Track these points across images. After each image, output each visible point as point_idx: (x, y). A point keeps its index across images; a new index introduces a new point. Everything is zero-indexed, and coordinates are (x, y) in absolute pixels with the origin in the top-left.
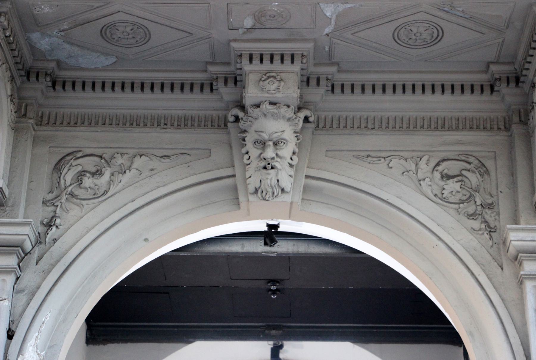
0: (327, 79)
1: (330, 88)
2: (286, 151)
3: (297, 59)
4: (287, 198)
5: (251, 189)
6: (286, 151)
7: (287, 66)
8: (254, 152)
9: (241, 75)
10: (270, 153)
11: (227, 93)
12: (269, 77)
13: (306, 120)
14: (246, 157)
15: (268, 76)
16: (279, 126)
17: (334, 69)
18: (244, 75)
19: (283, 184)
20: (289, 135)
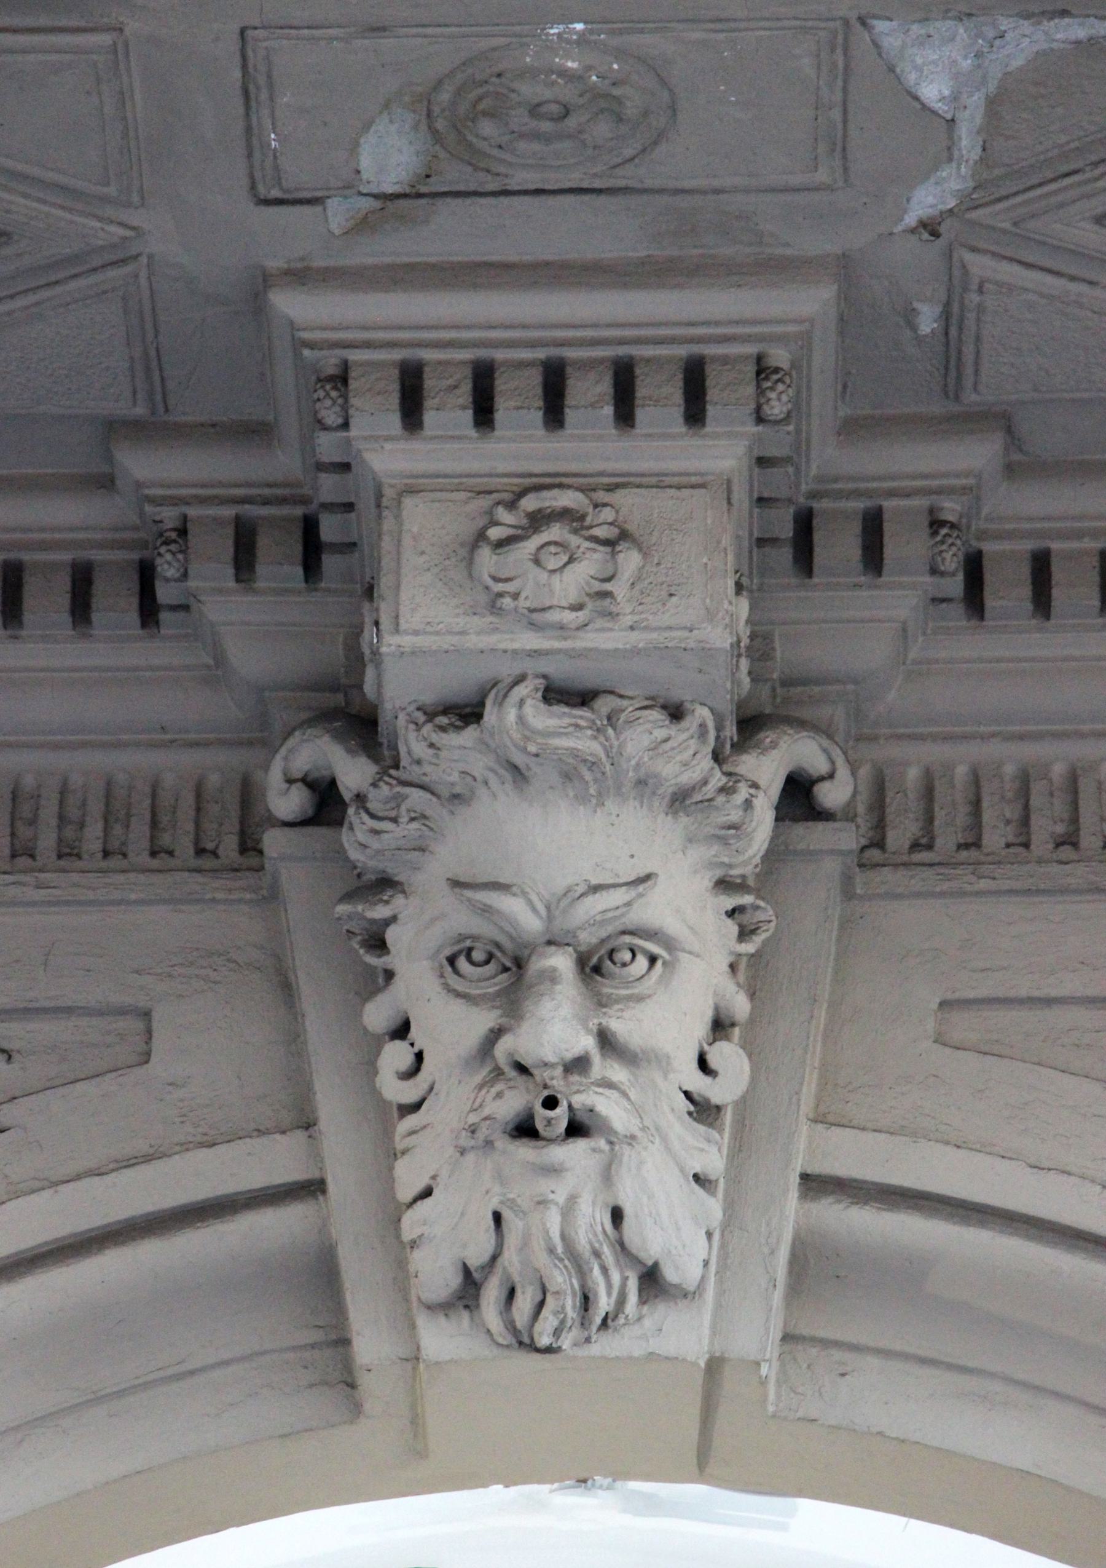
0: (936, 524)
1: (955, 585)
2: (668, 1016)
3: (728, 397)
4: (680, 1334)
5: (434, 1272)
6: (668, 1016)
7: (661, 441)
8: (450, 1025)
9: (349, 507)
10: (556, 1026)
11: (254, 628)
12: (538, 520)
13: (799, 797)
14: (396, 1055)
15: (525, 511)
16: (624, 849)
17: (975, 455)
18: (365, 504)
19: (651, 1239)
20: (682, 901)
